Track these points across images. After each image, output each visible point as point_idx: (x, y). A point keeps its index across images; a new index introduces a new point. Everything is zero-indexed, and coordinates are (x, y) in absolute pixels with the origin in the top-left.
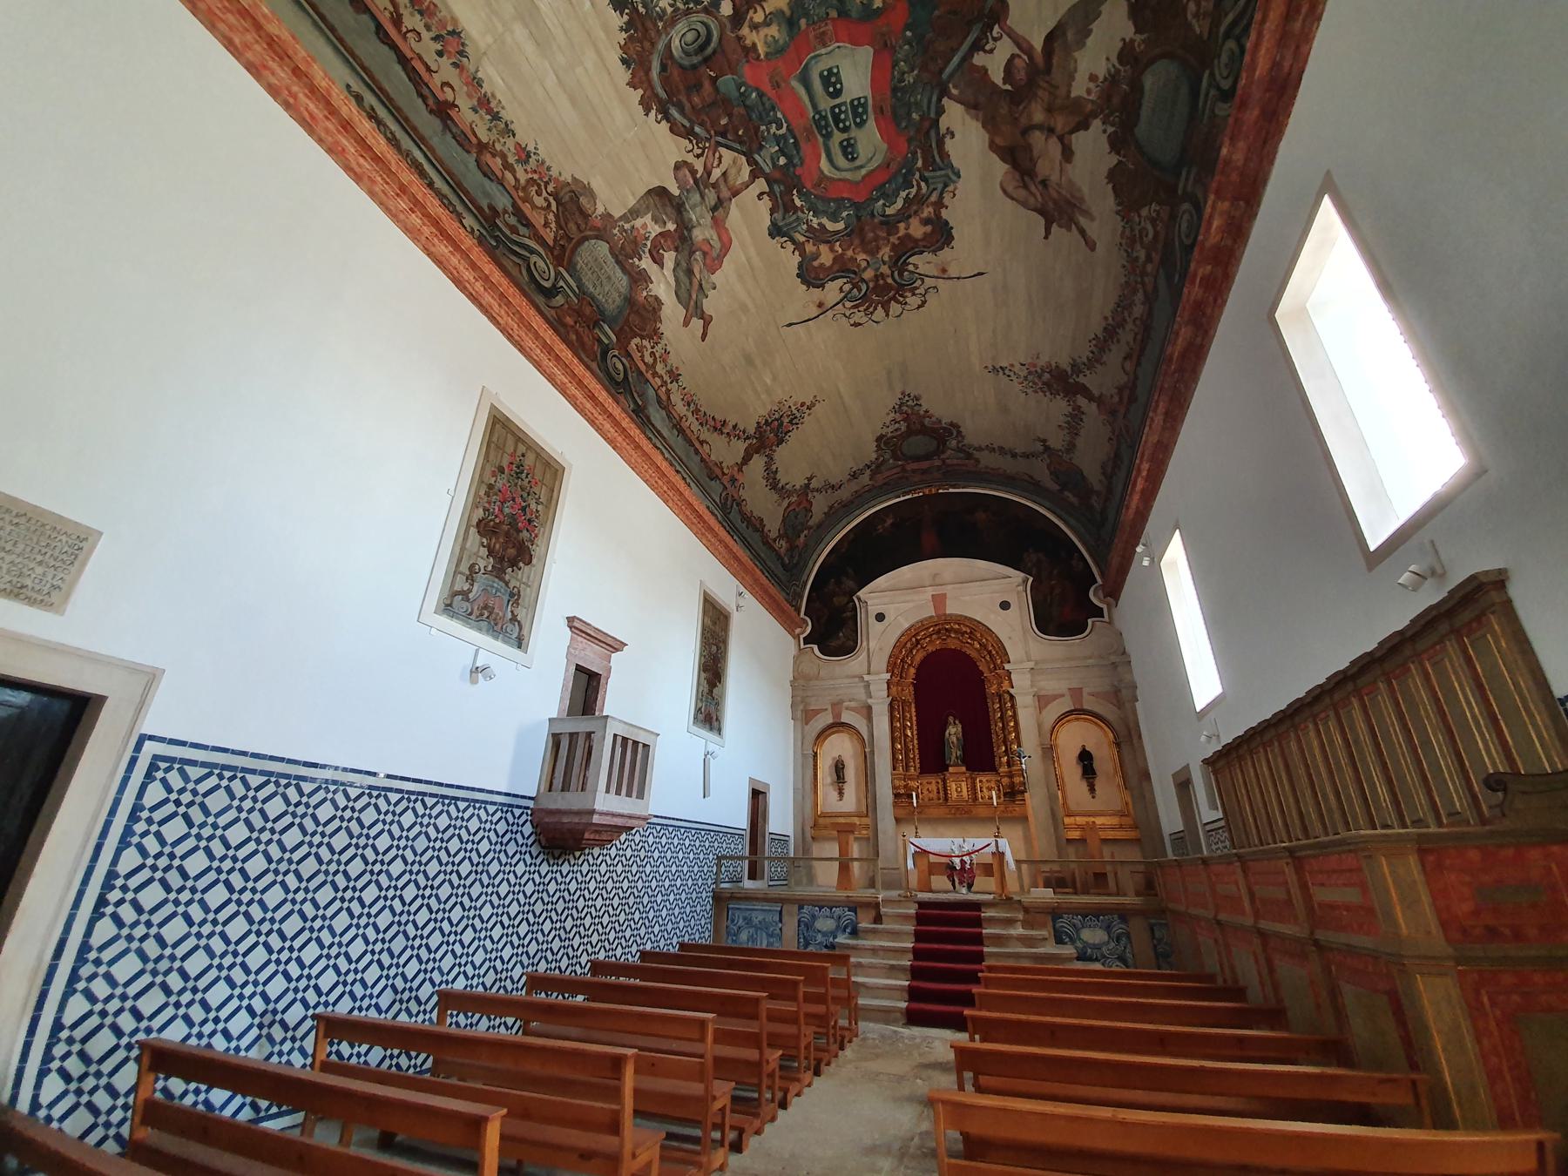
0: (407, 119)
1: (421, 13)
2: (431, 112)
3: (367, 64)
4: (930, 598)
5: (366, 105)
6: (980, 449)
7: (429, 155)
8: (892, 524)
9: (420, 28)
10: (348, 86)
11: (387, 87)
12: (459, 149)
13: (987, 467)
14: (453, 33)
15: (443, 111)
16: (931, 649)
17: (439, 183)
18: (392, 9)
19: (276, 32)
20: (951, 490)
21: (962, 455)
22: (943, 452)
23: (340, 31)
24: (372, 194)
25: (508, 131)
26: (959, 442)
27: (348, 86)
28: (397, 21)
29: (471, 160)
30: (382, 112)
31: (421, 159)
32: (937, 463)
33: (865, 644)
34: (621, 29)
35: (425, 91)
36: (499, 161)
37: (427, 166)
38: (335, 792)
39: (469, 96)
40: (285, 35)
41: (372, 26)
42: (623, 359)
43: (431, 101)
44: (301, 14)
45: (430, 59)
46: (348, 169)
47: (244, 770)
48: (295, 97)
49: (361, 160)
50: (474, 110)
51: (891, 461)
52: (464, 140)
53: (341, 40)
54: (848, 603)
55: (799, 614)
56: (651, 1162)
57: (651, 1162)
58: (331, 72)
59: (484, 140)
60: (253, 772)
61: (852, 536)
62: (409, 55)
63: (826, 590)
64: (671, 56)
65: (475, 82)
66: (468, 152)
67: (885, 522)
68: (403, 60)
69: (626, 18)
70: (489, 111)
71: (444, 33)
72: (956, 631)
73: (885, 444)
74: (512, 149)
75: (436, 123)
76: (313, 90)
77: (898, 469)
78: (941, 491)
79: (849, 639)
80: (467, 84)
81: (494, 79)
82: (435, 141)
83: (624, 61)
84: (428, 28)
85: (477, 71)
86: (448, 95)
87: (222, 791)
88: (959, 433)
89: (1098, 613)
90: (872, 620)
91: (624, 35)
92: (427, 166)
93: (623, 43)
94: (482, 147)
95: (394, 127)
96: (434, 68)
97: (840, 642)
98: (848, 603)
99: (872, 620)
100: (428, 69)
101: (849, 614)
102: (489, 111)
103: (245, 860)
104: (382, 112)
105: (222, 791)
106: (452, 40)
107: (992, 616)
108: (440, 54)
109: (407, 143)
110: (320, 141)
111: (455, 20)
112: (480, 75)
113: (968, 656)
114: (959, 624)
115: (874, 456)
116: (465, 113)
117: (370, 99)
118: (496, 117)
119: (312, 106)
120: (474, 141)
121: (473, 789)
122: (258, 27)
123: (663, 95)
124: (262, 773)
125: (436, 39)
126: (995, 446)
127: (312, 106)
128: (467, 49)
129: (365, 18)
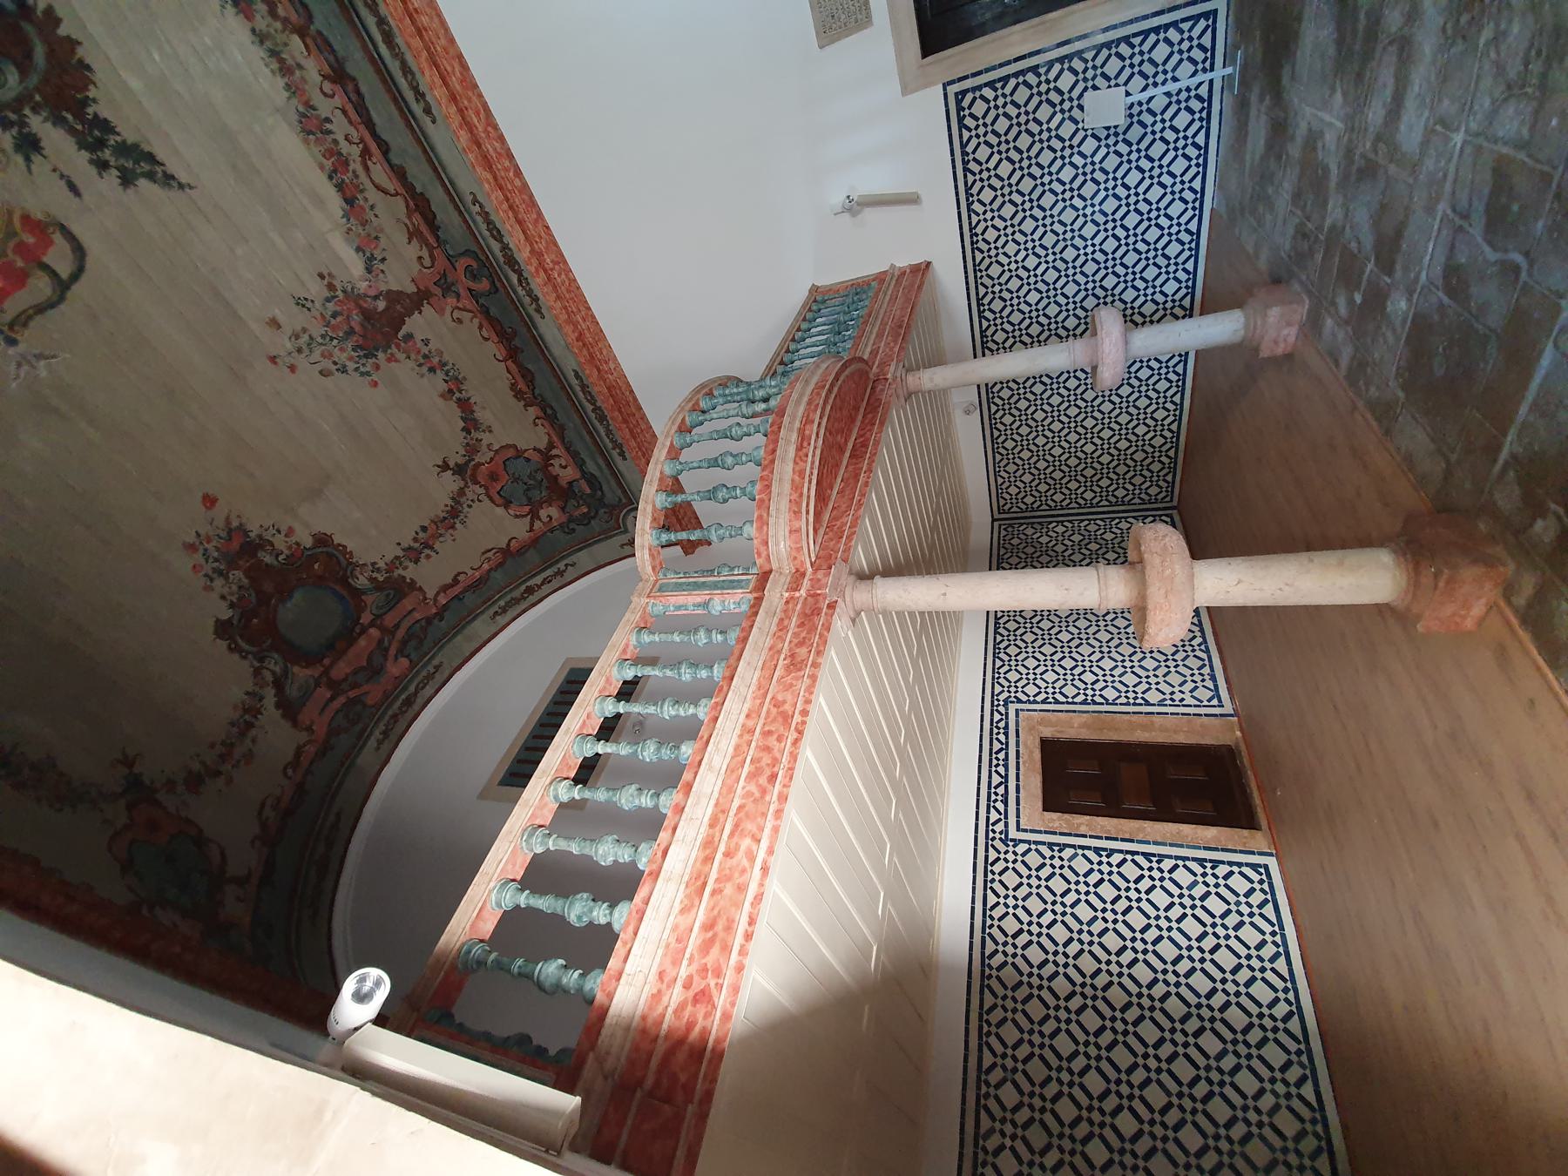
0: (384, 81)
1: (340, 154)
2: (354, 79)
3: (408, 132)
5: (422, 104)
7: (370, 46)
9: (343, 144)
10: (434, 122)
11: (396, 113)
12: (331, 39)
14: (310, 133)
15: (338, 75)
17: (371, 22)
18: (369, 163)
19: (484, 173)
23: (423, 159)
24: (452, 41)
25: (261, 37)
27: (434, 122)
28: (365, 153)
29: (318, 24)
30: (409, 95)
31: (383, 49)
34: (94, 100)
35: (354, 97)
36: (281, 11)
37: (378, 38)
38: (993, 873)
39: (303, 80)
40: (479, 169)
41: (391, 156)
43: (350, 87)
44: (452, 175)
45: (338, 118)
46: (464, 66)
47: (989, 787)
48: (486, 131)
49: (449, 69)
50: (300, 66)
52: (322, 45)
53: (425, 151)
58: (447, 137)
59: (296, 39)
60: (987, 857)
62: (362, 128)
64: (18, 66)
65: (294, 89)
66: (320, 33)
68: (370, 125)
69: (90, 110)
70: (281, 61)
71: (319, 135)
74: (258, 17)
75: (351, 69)
76: (470, 128)
80: (304, 91)
81: (271, 86)
82: (358, 55)
83: (88, 68)
84: (335, 142)
85: (289, 98)
86: (327, 87)
87: (1002, 132)
91: (91, 94)
92: (378, 38)
93: (91, 87)
94: (302, 33)
95: (403, 83)
96: (338, 112)
100: (344, 112)
102: (281, 61)
103: (1032, 95)
104: (409, 95)
105: (1002, 132)
106: (311, 126)
108: (328, 120)
109: (394, 66)
110: (480, 96)
111: (306, 142)
112: (286, 94)
116: (313, 70)
117: (417, 109)
118: (274, 53)
119: (475, 120)
120: (309, 41)
121: (957, 194)
122: (495, 178)
123: (29, 29)
124: (988, 812)
125: (329, 132)
127: (475, 120)
128: (296, 117)
129: (395, 161)
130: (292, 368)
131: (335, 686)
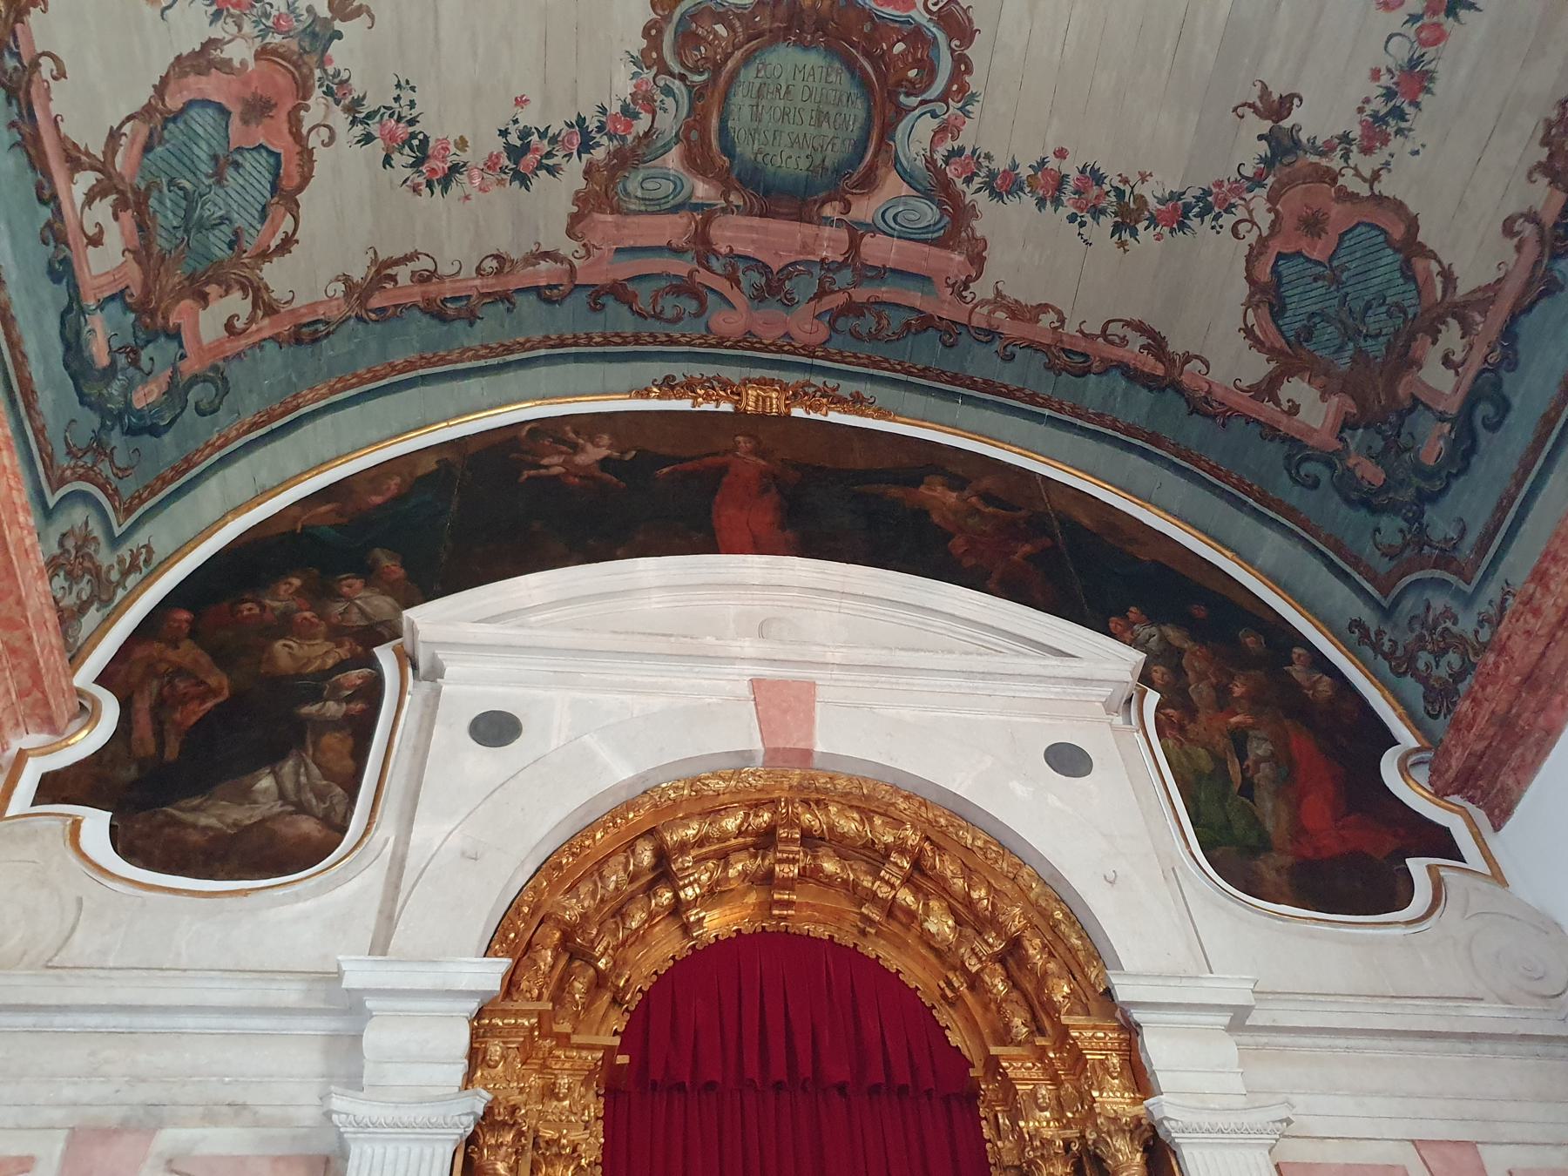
4: (744, 689)
6: (1003, 185)
8: (605, 463)
13: (999, 300)
16: (715, 922)
20: (835, 417)
21: (927, 213)
22: (868, 183)
26: (942, 132)
32: (829, 243)
33: (386, 832)
42: (29, 148)
51: (673, 160)
54: (342, 666)
55: (75, 659)
56: (1465, 862)
57: (1465, 862)
61: (430, 464)
63: (248, 609)
67: (576, 448)
72: (842, 846)
73: (687, 39)
77: (675, 228)
78: (798, 412)
79: (301, 809)
88: (962, 65)
89: (1440, 844)
90: (451, 732)
97: (242, 815)
98: (342, 666)
99: (451, 732)
101: (333, 709)
107: (1019, 789)
113: (893, 979)
114: (866, 815)
115: (623, 86)
126: (1070, 168)
130: (407, 82)
131: (702, 245)
